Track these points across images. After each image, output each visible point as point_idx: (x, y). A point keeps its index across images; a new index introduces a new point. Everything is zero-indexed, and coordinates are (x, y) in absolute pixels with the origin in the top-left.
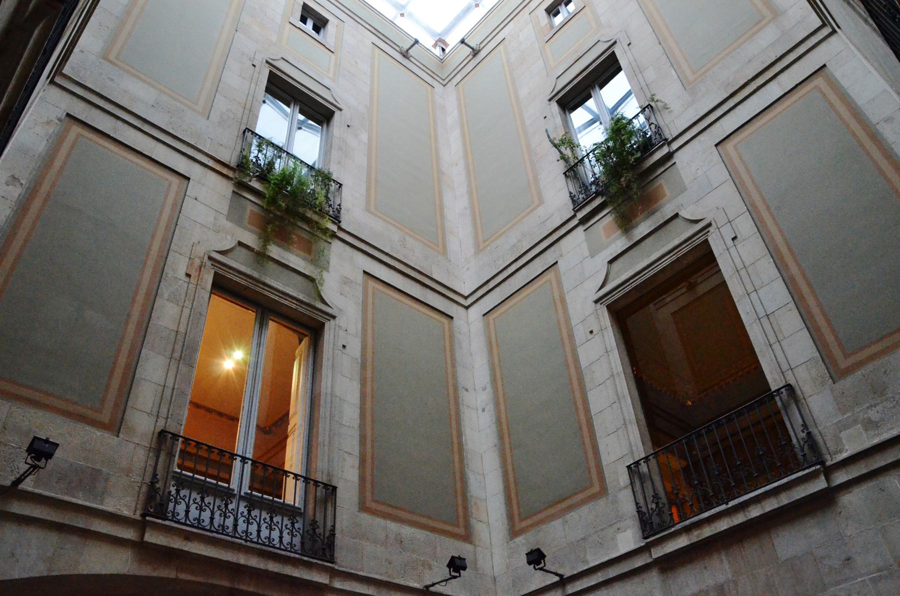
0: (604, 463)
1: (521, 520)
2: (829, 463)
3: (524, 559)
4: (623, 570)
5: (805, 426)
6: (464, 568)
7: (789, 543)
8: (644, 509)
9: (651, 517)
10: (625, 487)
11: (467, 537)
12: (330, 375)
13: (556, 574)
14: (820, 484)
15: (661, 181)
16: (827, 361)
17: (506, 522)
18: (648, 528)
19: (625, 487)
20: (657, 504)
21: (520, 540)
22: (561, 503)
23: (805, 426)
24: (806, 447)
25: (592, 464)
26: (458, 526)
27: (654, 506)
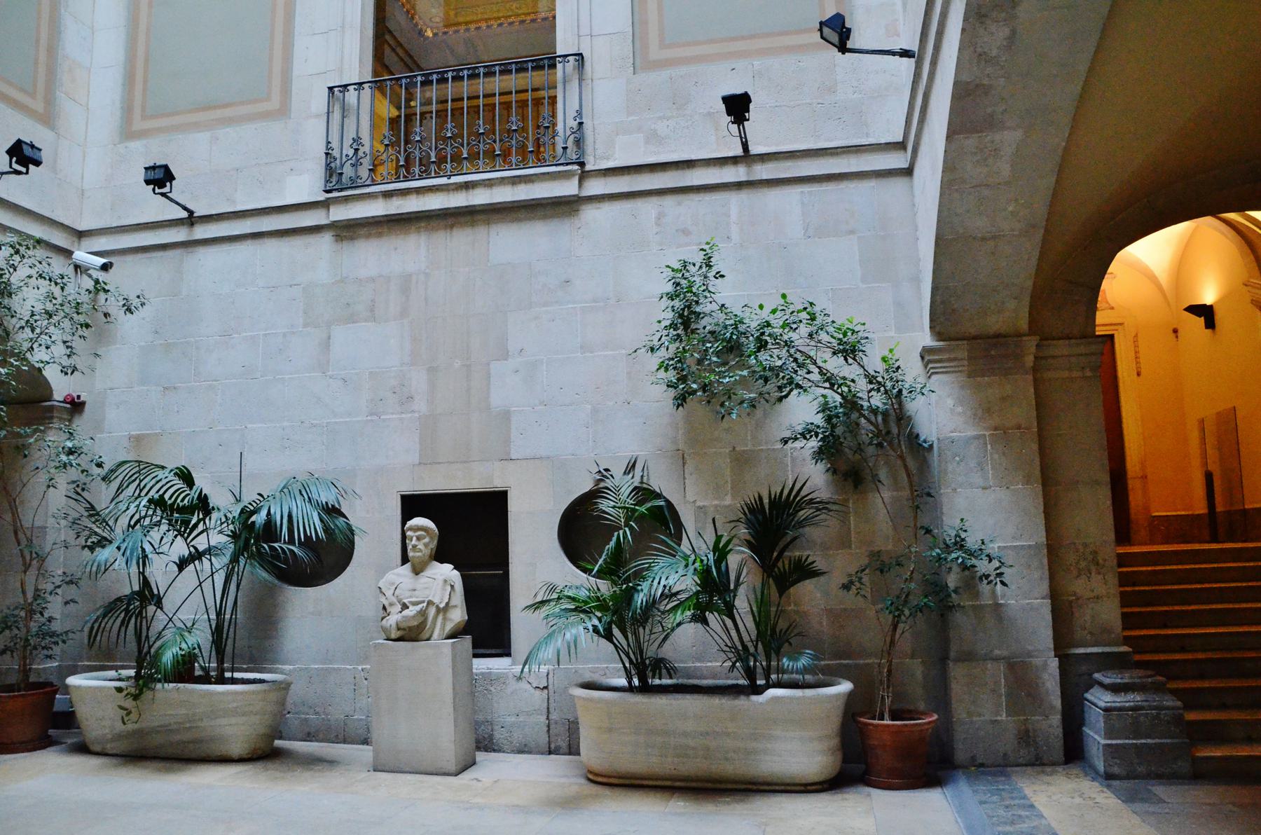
0: (296, 73)
1: (144, 117)
2: (588, 168)
3: (141, 175)
4: (274, 225)
5: (580, 113)
6: (38, 163)
7: (507, 242)
8: (336, 153)
9: (342, 166)
10: (317, 116)
11: (48, 118)
12: (1209, 451)
13: (185, 208)
14: (568, 188)
15: (583, 207)
16: (638, 45)
17: (118, 114)
18: (334, 179)
19: (317, 116)
20: (356, 150)
21: (136, 145)
22: (215, 111)
23: (580, 113)
24: (571, 139)
25: (277, 68)
26: (32, 95)
27: (351, 152)
